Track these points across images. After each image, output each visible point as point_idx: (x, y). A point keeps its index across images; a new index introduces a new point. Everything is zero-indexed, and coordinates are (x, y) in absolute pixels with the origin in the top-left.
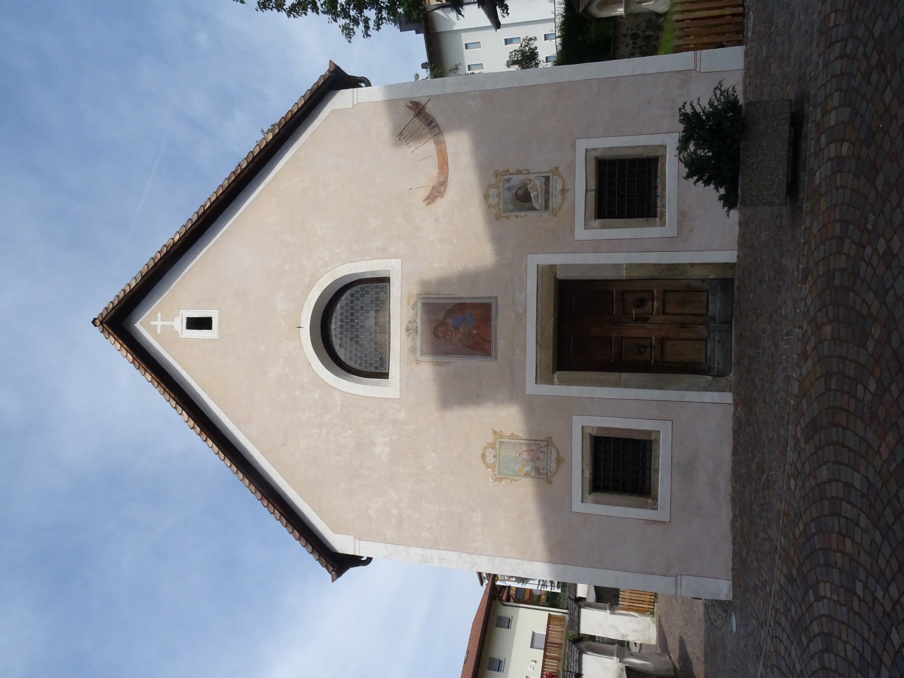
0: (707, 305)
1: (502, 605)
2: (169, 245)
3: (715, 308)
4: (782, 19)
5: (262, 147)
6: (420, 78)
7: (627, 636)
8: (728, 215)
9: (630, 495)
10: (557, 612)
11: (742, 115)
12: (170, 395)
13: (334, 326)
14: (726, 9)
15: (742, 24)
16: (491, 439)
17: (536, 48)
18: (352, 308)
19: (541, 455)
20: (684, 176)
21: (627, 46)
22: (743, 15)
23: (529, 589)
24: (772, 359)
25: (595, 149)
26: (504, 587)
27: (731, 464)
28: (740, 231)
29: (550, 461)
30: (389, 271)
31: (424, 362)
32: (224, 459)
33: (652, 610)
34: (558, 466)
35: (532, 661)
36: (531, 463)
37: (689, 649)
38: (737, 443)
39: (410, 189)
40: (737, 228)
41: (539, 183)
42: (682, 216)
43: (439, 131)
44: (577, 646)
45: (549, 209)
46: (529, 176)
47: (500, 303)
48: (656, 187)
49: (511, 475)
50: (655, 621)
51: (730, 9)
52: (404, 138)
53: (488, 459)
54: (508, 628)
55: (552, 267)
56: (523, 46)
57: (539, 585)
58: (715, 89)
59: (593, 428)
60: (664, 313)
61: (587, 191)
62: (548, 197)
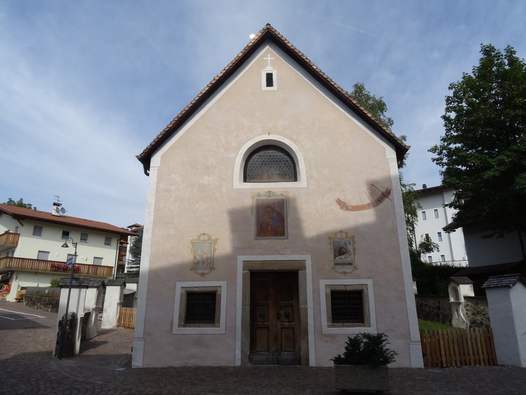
0: (286, 351)
1: (118, 240)
2: (310, 63)
3: (286, 355)
4: (434, 386)
5: (364, 111)
6: (413, 186)
7: (106, 312)
8: (331, 360)
9: (186, 313)
10: (114, 271)
11: (381, 366)
12: (231, 66)
13: (271, 152)
14: (445, 358)
15: (437, 366)
16: (213, 238)
17: (433, 251)
18: (280, 161)
19: (205, 265)
20: (350, 337)
21: (434, 304)
22: (442, 366)
23: (126, 254)
24: (258, 385)
25: (367, 289)
26: (127, 240)
27: (203, 366)
28: (326, 367)
29: (202, 270)
30: (353, 87)
31: (253, 201)
32: (198, 97)
33: (120, 326)
34: (199, 274)
35: (87, 258)
36: (201, 259)
37: (102, 347)
38: (214, 369)
39: (344, 191)
40: (328, 366)
41: (349, 259)
42: (333, 337)
43: (375, 205)
44: (101, 285)
45: (335, 265)
46: (352, 254)
47: (285, 240)
48: (348, 322)
49: (194, 248)
50: (114, 328)
51: (445, 360)
52: (371, 187)
53: (203, 236)
54: (105, 244)
55: (304, 268)
56: (434, 244)
57: (129, 260)
58: (394, 352)
59: (221, 292)
60: (282, 328)
61: (345, 285)
62: (341, 265)
